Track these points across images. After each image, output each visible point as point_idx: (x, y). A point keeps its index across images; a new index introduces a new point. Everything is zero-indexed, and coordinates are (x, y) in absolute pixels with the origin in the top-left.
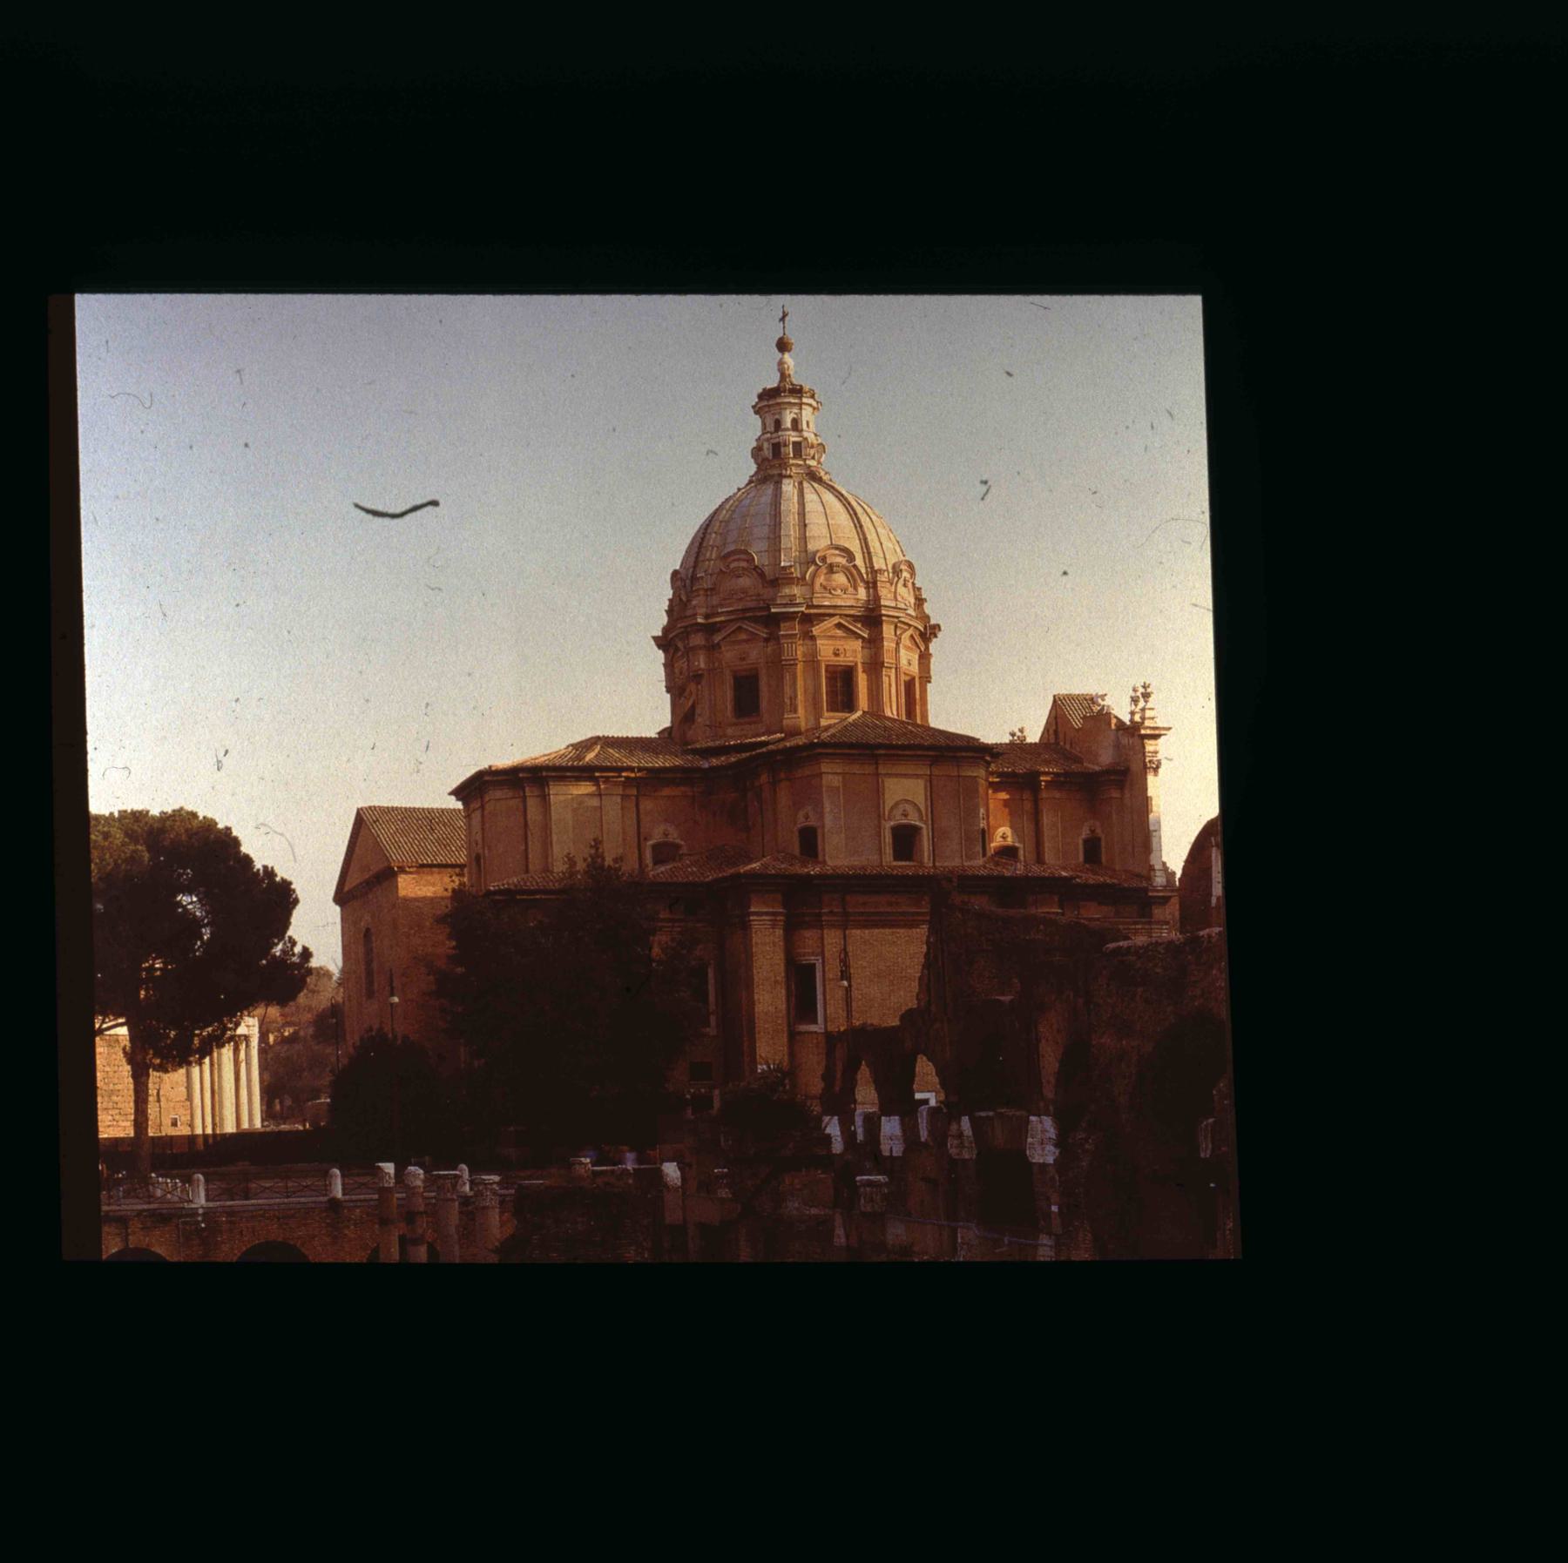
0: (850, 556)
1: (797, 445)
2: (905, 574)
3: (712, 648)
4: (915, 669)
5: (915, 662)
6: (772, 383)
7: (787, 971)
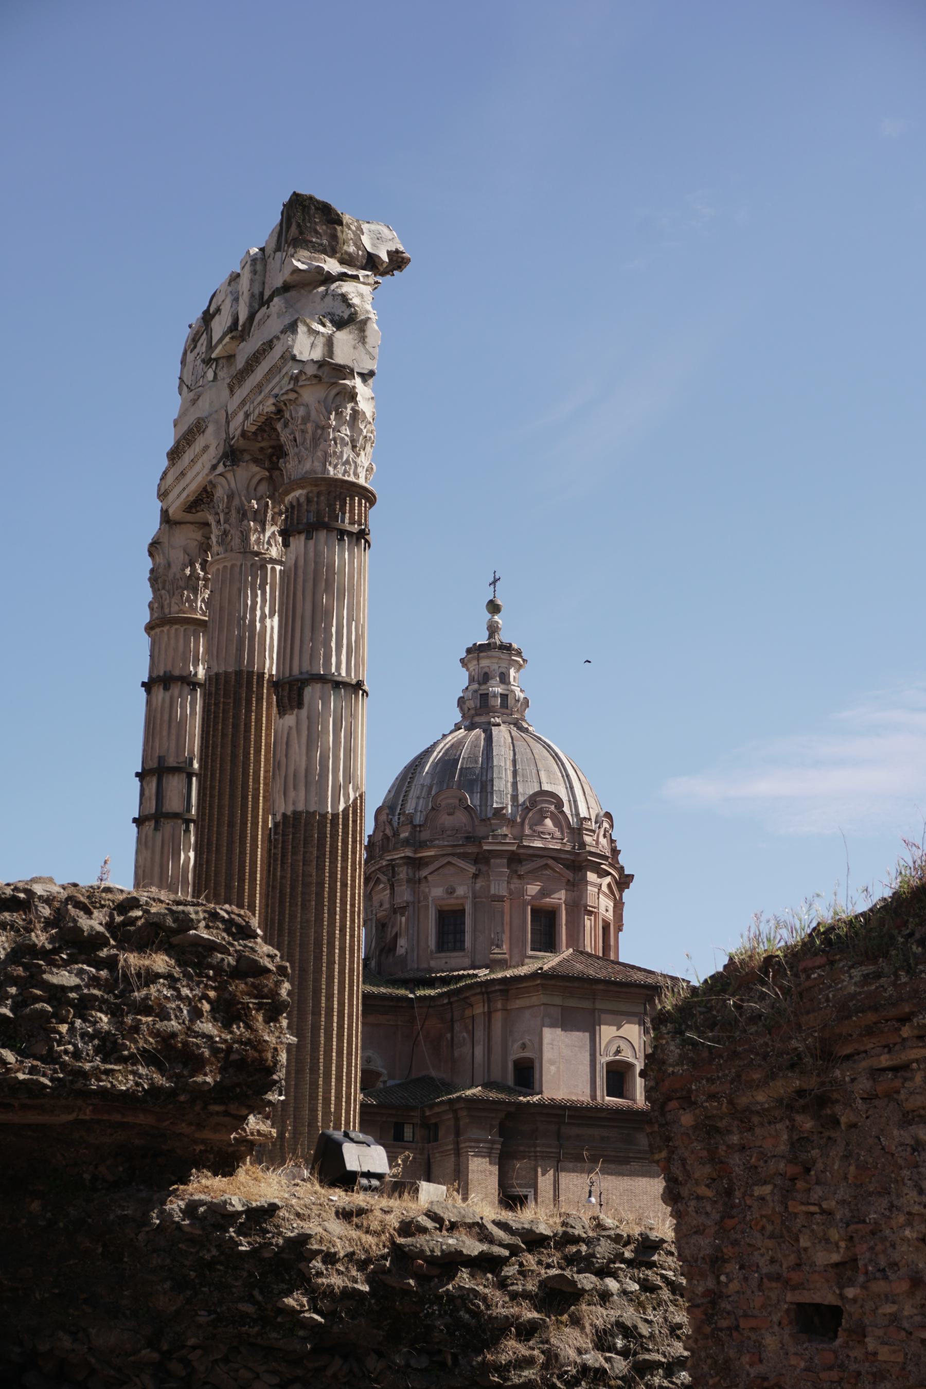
0: (559, 804)
1: (504, 697)
2: (606, 825)
3: (415, 882)
4: (610, 915)
5: (611, 909)
6: (483, 640)
7: (307, 1234)
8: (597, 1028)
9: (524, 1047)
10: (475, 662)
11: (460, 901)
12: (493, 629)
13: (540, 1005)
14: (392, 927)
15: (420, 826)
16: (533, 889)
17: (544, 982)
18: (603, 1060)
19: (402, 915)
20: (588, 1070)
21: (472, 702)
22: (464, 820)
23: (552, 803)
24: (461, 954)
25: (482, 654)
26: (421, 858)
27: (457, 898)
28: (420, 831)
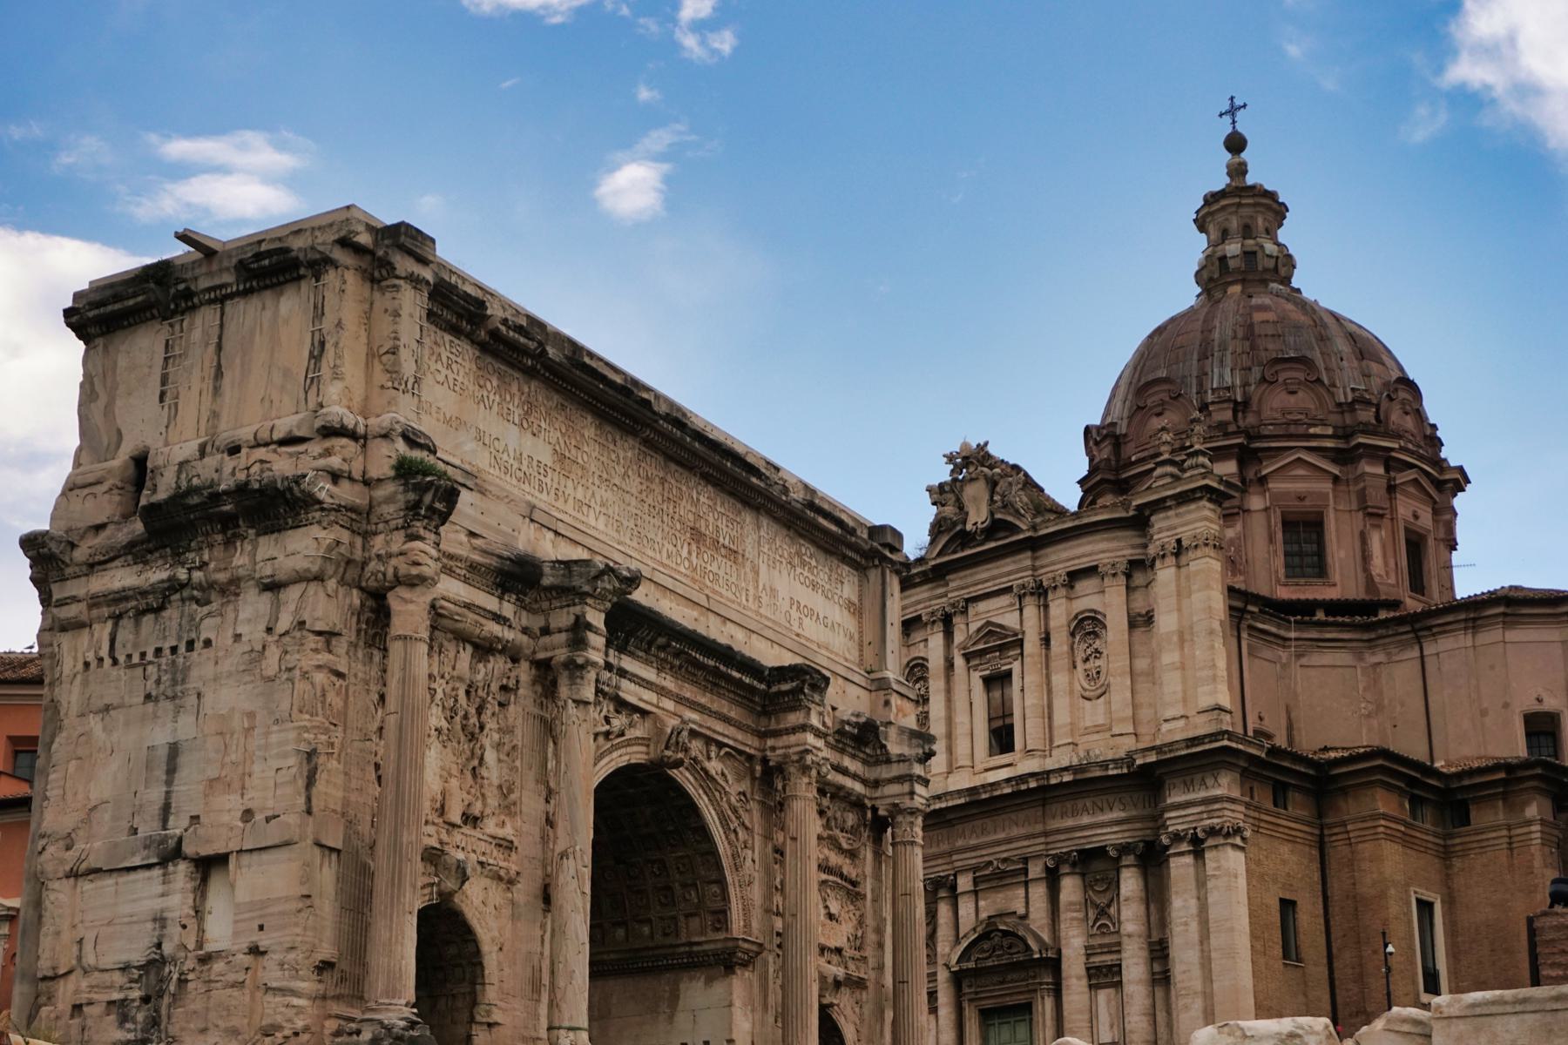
6: (1220, 181)
12: (1238, 171)
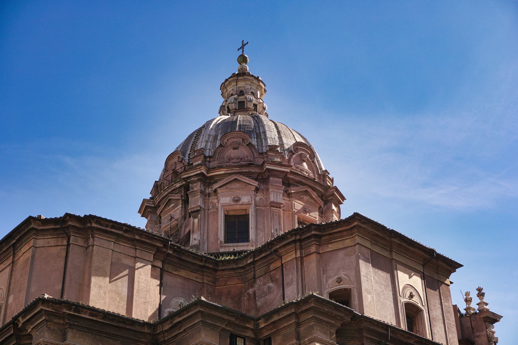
8: (395, 272)
9: (339, 281)
10: (234, 84)
11: (244, 207)
13: (355, 245)
14: (186, 227)
15: (210, 157)
16: (298, 205)
17: (360, 224)
18: (403, 300)
19: (195, 217)
20: (393, 306)
21: (233, 105)
22: (246, 153)
23: (308, 153)
24: (246, 244)
25: (240, 78)
26: (212, 177)
27: (242, 204)
28: (209, 162)
